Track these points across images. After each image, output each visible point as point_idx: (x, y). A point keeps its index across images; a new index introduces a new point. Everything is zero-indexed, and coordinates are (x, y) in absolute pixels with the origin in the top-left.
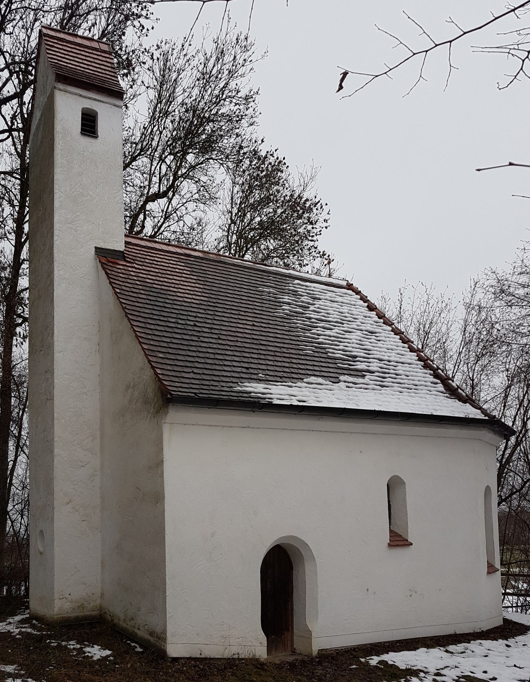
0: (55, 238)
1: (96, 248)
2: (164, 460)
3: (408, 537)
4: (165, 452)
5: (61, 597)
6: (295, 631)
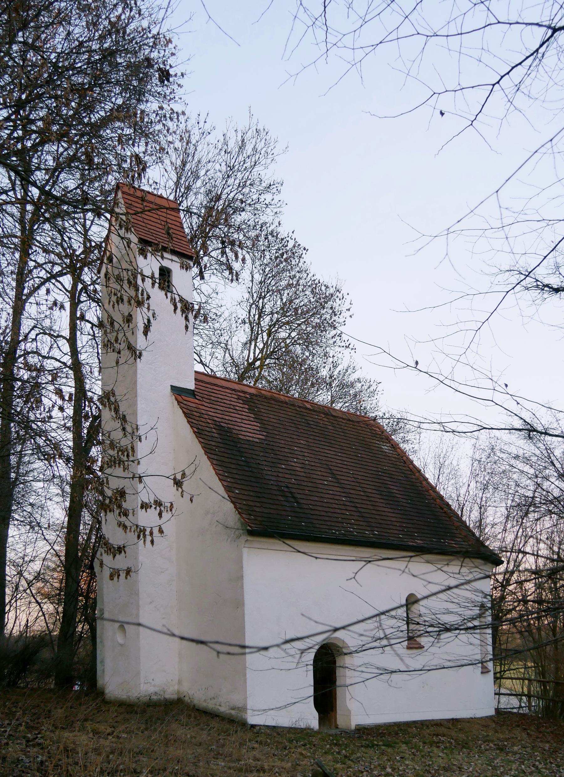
0: (138, 376)
1: (172, 386)
2: (244, 575)
3: (138, 521)
4: (244, 569)
5: (146, 682)
6: (338, 711)
